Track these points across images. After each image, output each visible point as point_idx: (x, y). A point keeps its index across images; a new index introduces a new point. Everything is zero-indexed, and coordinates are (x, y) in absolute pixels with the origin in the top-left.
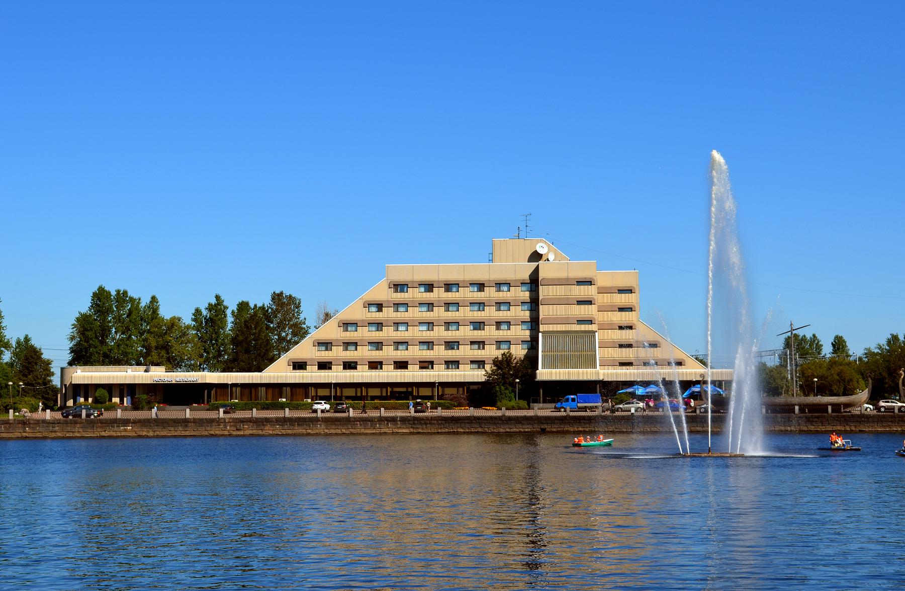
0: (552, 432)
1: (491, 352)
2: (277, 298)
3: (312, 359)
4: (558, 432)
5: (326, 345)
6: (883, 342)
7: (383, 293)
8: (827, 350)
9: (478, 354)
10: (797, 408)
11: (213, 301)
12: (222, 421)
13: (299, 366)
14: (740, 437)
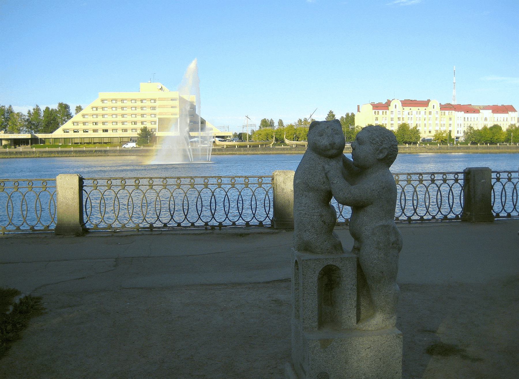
0: (111, 156)
1: (140, 126)
2: (61, 105)
3: (80, 129)
4: (86, 156)
5: (77, 123)
6: (297, 121)
7: (97, 103)
8: (276, 124)
9: (134, 126)
10: (248, 146)
11: (35, 107)
12: (35, 152)
13: (66, 131)
14: (457, 154)
